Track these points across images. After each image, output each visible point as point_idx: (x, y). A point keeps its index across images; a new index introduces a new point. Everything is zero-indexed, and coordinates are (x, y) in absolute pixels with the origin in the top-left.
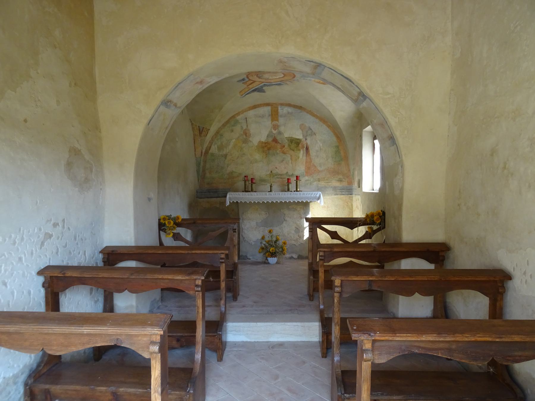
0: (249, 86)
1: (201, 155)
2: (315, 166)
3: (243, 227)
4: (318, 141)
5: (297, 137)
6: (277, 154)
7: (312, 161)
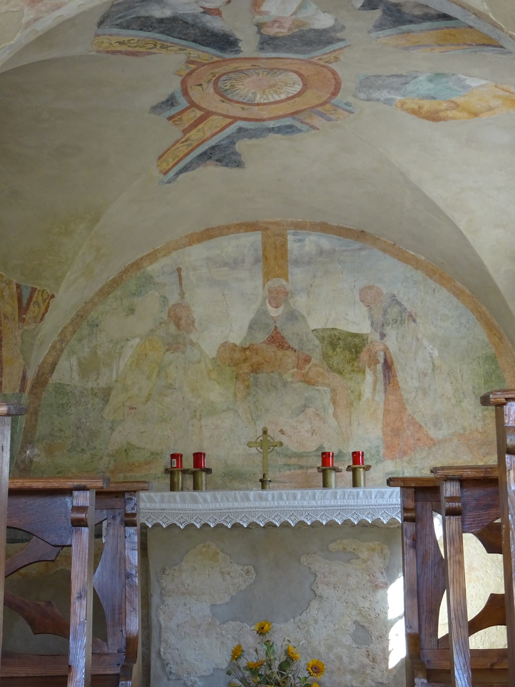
0: (188, 135)
1: (22, 389)
2: (417, 423)
3: (162, 621)
4: (425, 342)
5: (353, 329)
6: (285, 384)
7: (405, 409)
